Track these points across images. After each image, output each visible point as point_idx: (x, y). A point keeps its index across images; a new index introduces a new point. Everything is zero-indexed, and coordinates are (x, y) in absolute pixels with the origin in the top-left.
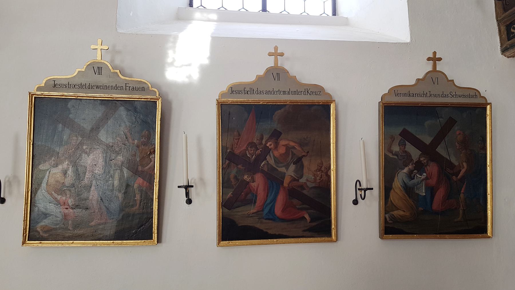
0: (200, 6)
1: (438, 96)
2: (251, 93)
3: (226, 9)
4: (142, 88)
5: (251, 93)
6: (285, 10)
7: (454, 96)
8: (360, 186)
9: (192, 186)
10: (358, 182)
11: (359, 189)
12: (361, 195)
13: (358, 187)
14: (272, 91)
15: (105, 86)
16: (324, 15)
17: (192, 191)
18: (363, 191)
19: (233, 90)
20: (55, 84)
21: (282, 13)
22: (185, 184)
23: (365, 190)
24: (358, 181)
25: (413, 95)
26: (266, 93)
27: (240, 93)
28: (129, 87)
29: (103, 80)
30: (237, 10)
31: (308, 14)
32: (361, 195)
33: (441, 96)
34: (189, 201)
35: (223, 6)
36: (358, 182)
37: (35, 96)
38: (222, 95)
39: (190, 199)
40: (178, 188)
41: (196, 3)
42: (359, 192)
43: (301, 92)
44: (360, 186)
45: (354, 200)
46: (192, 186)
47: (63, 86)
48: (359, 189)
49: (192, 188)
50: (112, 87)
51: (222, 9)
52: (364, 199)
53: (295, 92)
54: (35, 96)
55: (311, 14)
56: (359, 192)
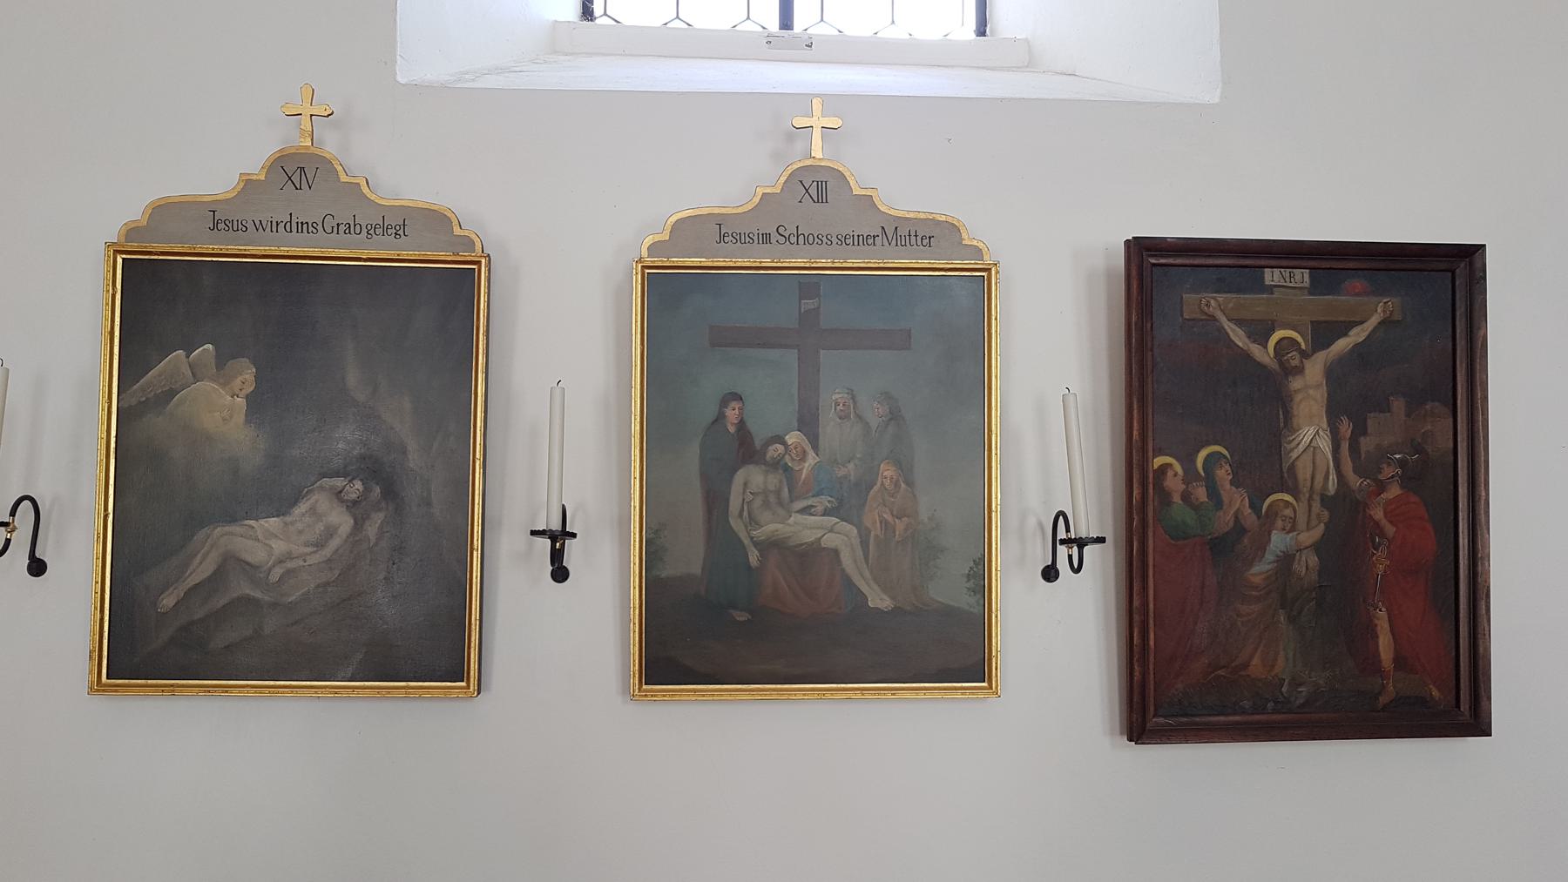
0: (607, 15)
1: (240, 226)
2: (856, 243)
3: (618, 22)
4: (398, 222)
5: (856, 243)
6: (678, 17)
7: (793, 239)
8: (1068, 530)
9: (574, 535)
10: (1061, 517)
11: (1063, 542)
12: (1070, 557)
13: (1062, 534)
14: (289, 224)
15: (858, 236)
16: (677, 24)
17: (572, 550)
18: (1075, 549)
19: (686, 230)
20: (216, 219)
21: (668, 25)
22: (556, 525)
23: (1081, 543)
24: (1061, 514)
25: (349, 227)
26: (347, 232)
27: (748, 239)
28: (930, 238)
29: (309, 206)
30: (659, 25)
31: (764, 28)
32: (1070, 557)
33: (364, 228)
34: (560, 574)
35: (608, 13)
36: (1061, 517)
37: (124, 256)
38: (653, 249)
39: (565, 567)
40: (1105, 538)
41: (598, 8)
42: (1062, 551)
43: (930, 238)
44: (1068, 530)
45: (1048, 566)
46: (574, 535)
47: (743, 237)
48: (1063, 542)
49: (574, 540)
50: (235, 229)
51: (677, 24)
52: (1077, 571)
53: (903, 244)
54: (124, 256)
55: (697, 25)
56: (1062, 551)
